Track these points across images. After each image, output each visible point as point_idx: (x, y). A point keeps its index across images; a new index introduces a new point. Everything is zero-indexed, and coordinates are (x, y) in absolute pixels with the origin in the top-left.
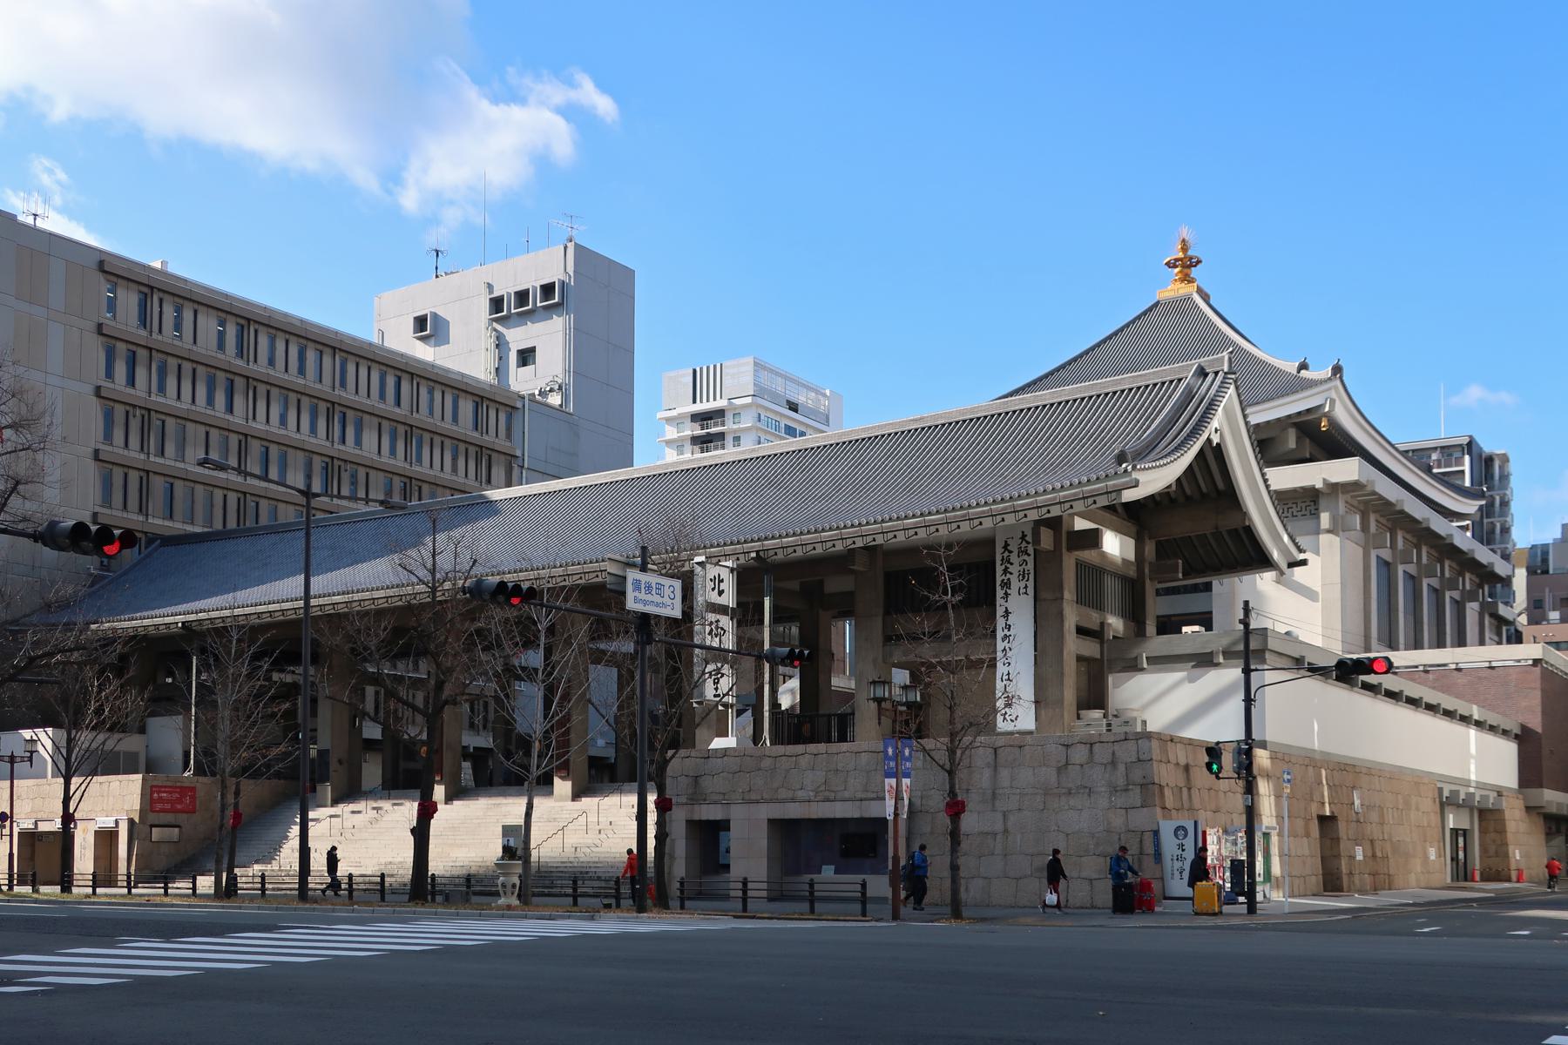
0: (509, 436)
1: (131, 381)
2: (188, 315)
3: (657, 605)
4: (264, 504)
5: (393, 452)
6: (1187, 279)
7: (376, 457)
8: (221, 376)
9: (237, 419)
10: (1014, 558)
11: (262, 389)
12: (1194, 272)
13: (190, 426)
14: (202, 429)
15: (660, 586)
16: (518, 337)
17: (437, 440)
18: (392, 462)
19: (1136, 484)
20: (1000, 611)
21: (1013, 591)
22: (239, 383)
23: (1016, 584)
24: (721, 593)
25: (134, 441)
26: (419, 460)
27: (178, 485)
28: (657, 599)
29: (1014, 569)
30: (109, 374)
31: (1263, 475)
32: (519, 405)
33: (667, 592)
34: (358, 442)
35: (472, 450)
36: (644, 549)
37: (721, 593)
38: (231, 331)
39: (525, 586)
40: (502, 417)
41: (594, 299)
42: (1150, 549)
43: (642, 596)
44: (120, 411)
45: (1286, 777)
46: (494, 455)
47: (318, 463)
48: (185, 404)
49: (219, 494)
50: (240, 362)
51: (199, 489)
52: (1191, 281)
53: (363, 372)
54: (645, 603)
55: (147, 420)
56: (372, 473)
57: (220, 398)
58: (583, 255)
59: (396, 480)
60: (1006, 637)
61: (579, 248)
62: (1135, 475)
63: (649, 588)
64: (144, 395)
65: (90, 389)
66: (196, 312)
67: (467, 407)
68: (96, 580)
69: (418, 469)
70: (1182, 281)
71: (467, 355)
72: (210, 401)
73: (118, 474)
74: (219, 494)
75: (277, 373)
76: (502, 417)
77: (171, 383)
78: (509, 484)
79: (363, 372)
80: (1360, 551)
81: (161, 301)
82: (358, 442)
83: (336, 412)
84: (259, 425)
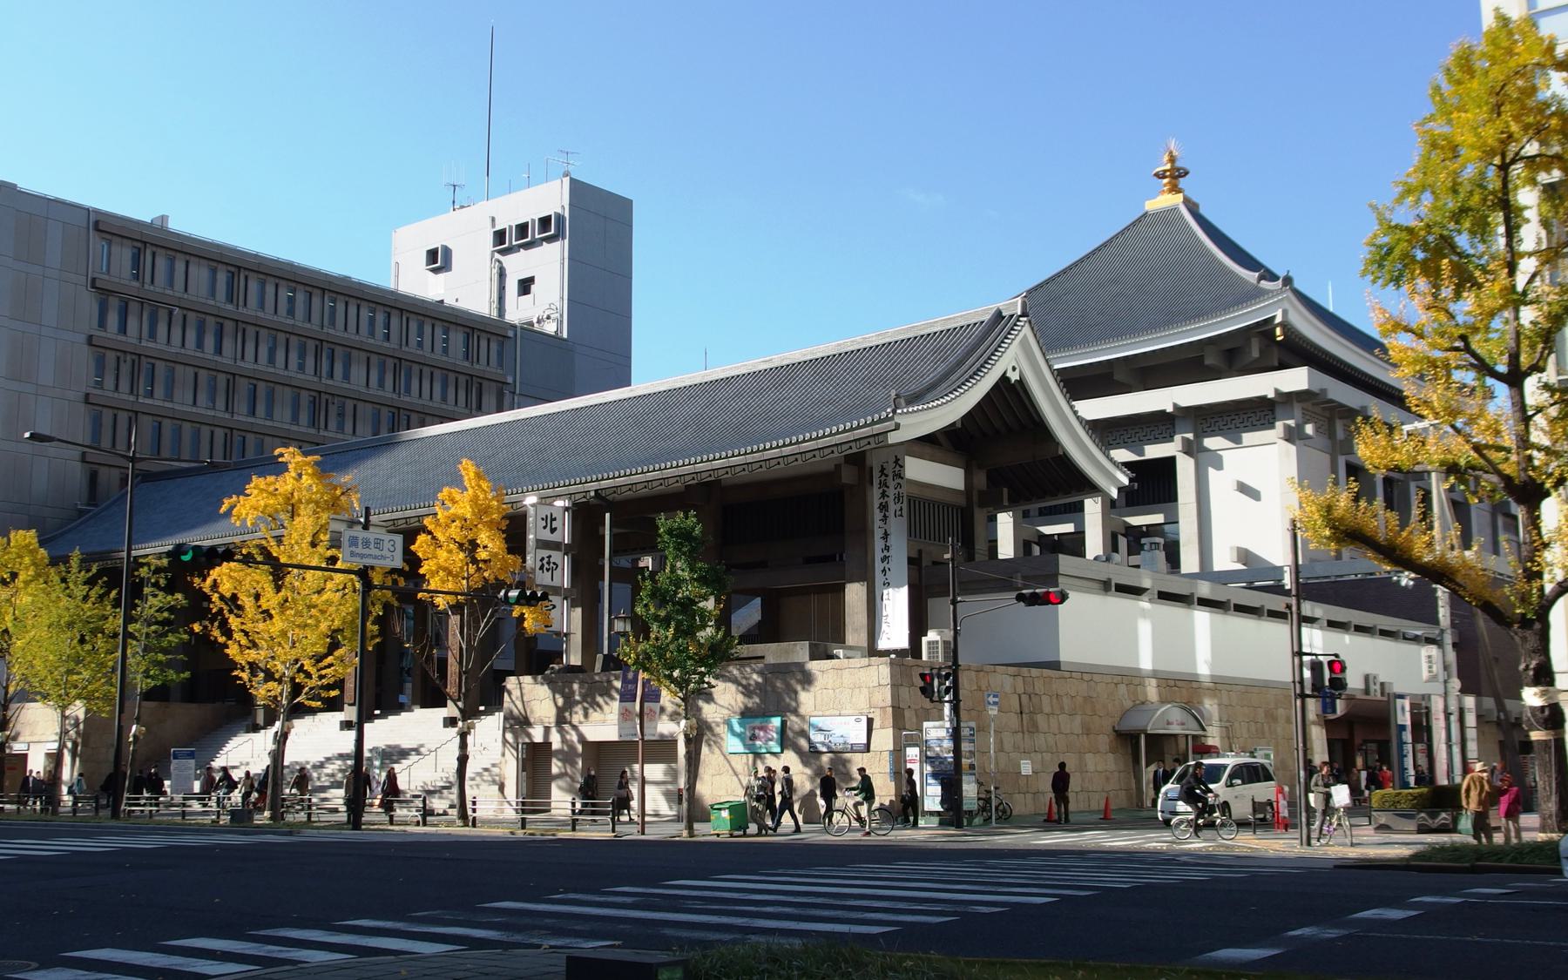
0: (500, 364)
1: (123, 329)
2: (180, 267)
3: (376, 557)
4: (250, 438)
5: (381, 384)
6: (1175, 189)
7: (363, 390)
8: (211, 321)
9: (226, 359)
10: (892, 484)
11: (251, 331)
12: (1182, 182)
13: (179, 368)
14: (191, 371)
15: (378, 542)
16: (518, 265)
17: (426, 370)
18: (380, 393)
19: (897, 427)
20: (878, 534)
21: (891, 513)
22: (229, 326)
23: (893, 507)
24: (553, 530)
25: (124, 385)
26: (408, 390)
27: (167, 423)
28: (377, 552)
29: (891, 492)
30: (102, 324)
31: (1072, 407)
32: (511, 334)
33: (387, 545)
34: (346, 377)
35: (462, 379)
36: (367, 509)
37: (553, 530)
38: (222, 277)
39: (220, 550)
40: (494, 346)
41: (597, 232)
42: (981, 480)
43: (359, 550)
44: (111, 356)
45: (991, 699)
46: (485, 383)
47: (305, 397)
48: (175, 348)
49: (206, 431)
50: (230, 307)
51: (187, 426)
52: (1179, 191)
53: (352, 310)
54: (362, 556)
55: (139, 366)
56: (360, 405)
57: (209, 342)
58: (579, 190)
59: (385, 410)
60: (884, 559)
61: (573, 182)
62: (897, 419)
63: (366, 543)
64: (135, 341)
65: (82, 338)
66: (187, 263)
67: (457, 338)
68: (81, 513)
69: (407, 399)
70: (1170, 191)
71: (465, 289)
72: (200, 344)
73: (107, 416)
74: (206, 431)
75: (267, 315)
76: (494, 346)
77: (162, 329)
78: (500, 410)
79: (352, 310)
80: (1326, 458)
81: (154, 254)
82: (346, 377)
83: (325, 349)
84: (248, 365)
